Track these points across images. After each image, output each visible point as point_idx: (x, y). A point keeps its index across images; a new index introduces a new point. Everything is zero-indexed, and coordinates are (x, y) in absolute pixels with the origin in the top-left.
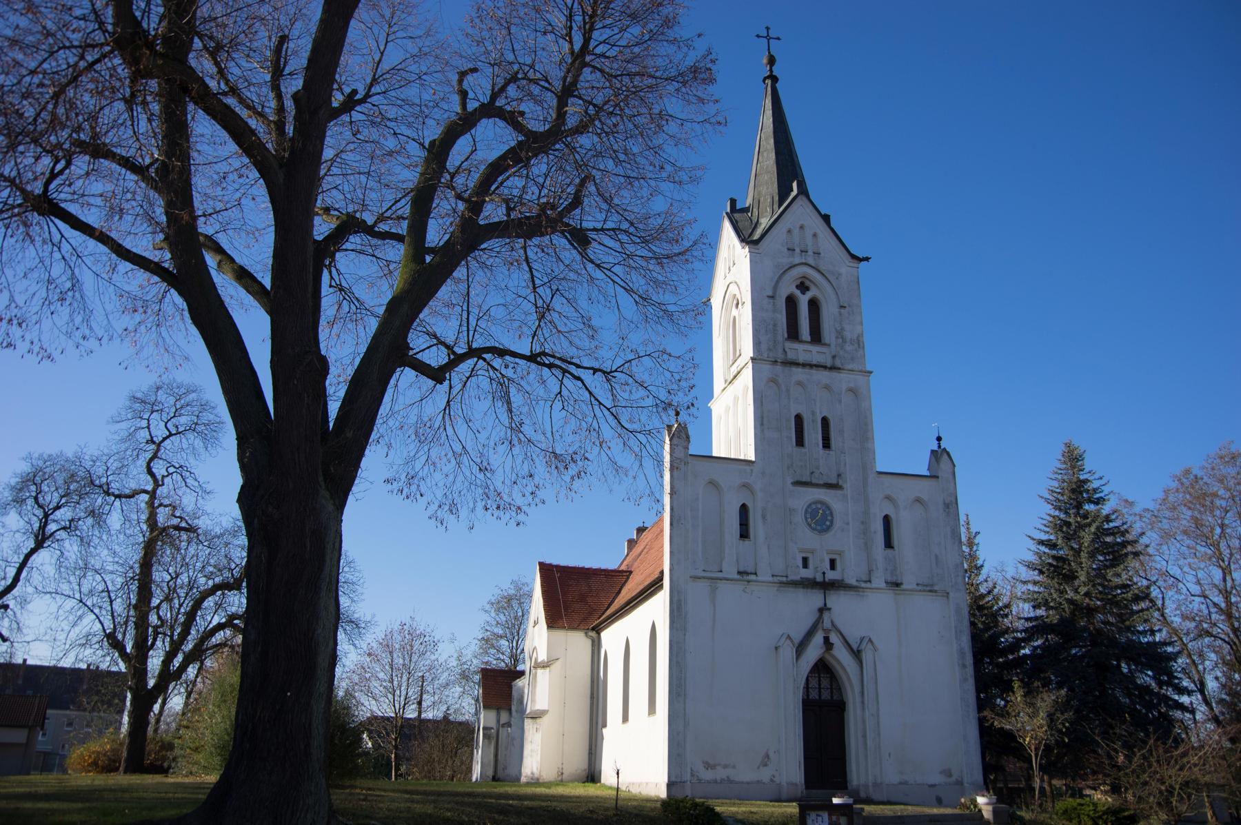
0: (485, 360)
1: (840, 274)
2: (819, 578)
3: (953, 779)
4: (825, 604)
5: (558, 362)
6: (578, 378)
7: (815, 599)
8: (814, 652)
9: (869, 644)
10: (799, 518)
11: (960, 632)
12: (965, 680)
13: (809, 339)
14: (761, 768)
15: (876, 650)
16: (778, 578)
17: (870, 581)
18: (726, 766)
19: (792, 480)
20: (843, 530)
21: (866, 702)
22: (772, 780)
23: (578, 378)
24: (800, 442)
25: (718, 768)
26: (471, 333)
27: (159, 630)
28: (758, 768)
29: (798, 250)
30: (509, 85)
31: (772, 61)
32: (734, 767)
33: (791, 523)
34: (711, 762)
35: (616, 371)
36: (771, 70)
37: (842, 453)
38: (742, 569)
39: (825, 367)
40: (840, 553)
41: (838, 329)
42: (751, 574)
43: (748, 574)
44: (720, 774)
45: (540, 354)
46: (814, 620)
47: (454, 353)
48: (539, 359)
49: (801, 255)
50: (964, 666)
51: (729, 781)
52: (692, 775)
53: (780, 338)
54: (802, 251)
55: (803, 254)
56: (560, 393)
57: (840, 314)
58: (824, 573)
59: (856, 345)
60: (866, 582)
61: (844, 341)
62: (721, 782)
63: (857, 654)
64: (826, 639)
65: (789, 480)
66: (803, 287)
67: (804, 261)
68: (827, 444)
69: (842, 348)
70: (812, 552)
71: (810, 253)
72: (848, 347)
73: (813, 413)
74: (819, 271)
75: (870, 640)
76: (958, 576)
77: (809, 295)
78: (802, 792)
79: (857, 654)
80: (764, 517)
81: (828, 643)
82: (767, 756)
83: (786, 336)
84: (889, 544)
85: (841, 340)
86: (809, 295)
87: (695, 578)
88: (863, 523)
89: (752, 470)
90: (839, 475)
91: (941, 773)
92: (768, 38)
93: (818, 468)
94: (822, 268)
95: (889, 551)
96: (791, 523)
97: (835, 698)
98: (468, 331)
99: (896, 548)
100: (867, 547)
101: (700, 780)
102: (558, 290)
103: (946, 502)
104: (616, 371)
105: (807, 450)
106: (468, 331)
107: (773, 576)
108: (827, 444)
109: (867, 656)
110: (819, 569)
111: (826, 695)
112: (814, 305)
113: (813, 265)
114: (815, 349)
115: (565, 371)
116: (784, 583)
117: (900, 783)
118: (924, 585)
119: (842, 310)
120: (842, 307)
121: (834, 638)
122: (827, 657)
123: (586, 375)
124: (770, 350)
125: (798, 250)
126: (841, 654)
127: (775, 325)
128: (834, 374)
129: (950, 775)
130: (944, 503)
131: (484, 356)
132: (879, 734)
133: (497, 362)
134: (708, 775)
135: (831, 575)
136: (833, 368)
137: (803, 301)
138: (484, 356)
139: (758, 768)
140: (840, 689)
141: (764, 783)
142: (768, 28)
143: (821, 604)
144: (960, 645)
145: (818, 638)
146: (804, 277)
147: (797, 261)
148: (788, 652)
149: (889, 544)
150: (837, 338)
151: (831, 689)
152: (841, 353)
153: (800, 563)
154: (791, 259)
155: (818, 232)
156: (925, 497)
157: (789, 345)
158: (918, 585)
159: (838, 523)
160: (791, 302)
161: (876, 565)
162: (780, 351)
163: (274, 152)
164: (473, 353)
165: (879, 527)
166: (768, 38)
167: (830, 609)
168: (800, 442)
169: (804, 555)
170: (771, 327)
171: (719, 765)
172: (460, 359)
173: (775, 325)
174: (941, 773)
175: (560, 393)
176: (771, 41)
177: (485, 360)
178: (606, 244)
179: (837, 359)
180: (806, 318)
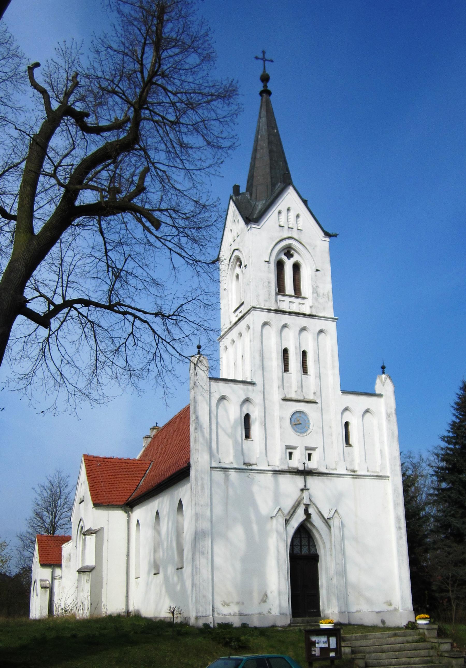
0: (76, 309)
1: (316, 246)
2: (301, 468)
4: (305, 486)
5: (129, 310)
6: (146, 322)
7: (299, 481)
8: (300, 517)
11: (397, 504)
12: (401, 538)
14: (262, 603)
23: (146, 322)
24: (286, 368)
26: (64, 288)
27: (199, 355)
30: (33, 75)
31: (265, 79)
35: (173, 315)
36: (265, 86)
39: (304, 315)
45: (115, 305)
47: (53, 304)
48: (115, 308)
49: (289, 230)
50: (400, 528)
54: (289, 228)
55: (290, 229)
56: (132, 333)
57: (316, 276)
58: (304, 464)
59: (327, 299)
61: (318, 295)
62: (234, 615)
63: (326, 521)
64: (306, 511)
66: (289, 255)
67: (290, 235)
71: (295, 229)
72: (321, 300)
74: (300, 243)
77: (293, 260)
78: (291, 620)
86: (293, 260)
92: (264, 60)
98: (63, 287)
102: (130, 256)
103: (389, 413)
104: (173, 315)
106: (63, 287)
109: (335, 523)
111: (305, 551)
112: (296, 267)
113: (297, 238)
114: (297, 301)
115: (135, 317)
118: (372, 472)
119: (317, 273)
120: (317, 270)
121: (311, 511)
122: (306, 523)
123: (149, 318)
124: (265, 301)
125: (286, 227)
126: (315, 519)
128: (311, 320)
129: (390, 605)
130: (387, 414)
131: (75, 305)
133: (84, 310)
138: (75, 305)
141: (264, 615)
142: (264, 52)
143: (302, 486)
150: (313, 293)
160: (280, 265)
164: (68, 304)
166: (264, 60)
167: (308, 489)
170: (267, 283)
172: (58, 308)
175: (132, 333)
176: (266, 62)
177: (76, 309)
179: (313, 308)
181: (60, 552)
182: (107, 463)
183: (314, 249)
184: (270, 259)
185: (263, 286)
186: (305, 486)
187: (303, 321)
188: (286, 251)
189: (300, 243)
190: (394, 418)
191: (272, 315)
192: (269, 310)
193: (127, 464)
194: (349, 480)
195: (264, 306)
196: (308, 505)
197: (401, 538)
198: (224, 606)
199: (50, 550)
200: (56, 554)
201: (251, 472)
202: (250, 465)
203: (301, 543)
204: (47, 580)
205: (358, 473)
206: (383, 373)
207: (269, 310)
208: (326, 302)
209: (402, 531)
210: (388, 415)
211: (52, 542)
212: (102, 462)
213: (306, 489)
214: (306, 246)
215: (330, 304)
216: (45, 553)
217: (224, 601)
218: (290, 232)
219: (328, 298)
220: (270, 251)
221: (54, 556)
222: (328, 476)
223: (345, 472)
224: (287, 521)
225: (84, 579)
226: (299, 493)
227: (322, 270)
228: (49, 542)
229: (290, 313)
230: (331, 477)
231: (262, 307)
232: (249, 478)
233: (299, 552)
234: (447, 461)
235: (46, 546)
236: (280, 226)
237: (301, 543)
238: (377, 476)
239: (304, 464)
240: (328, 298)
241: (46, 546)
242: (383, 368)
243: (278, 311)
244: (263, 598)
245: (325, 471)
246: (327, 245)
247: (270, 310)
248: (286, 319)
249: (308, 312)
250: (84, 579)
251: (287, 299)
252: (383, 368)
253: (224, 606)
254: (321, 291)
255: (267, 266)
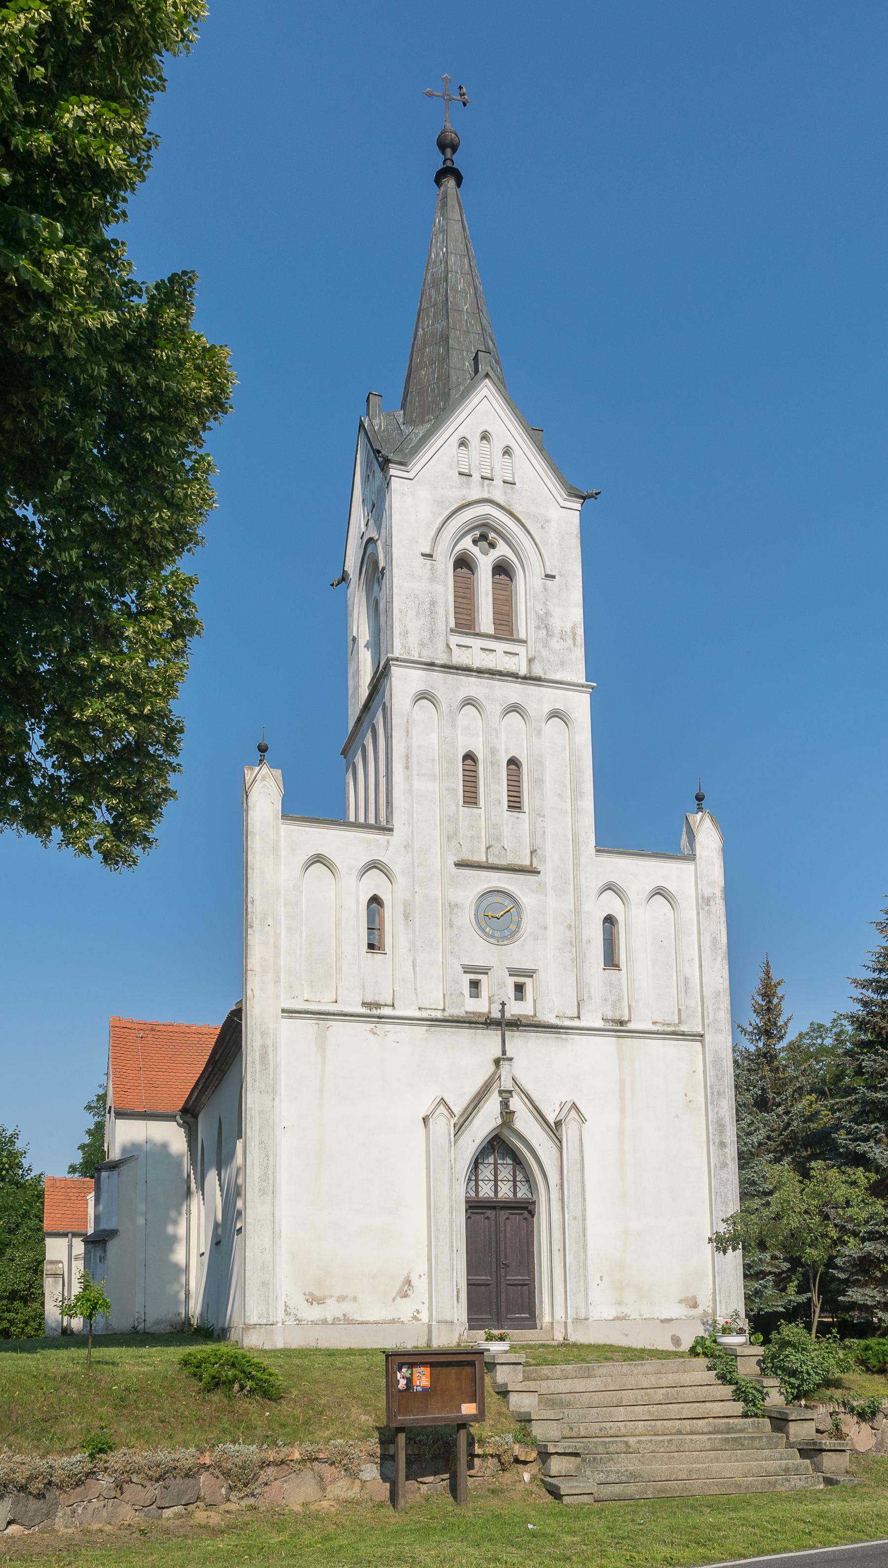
1: (547, 521)
3: (699, 1311)
4: (504, 1052)
9: (573, 1112)
10: (466, 917)
11: (719, 1093)
13: (491, 631)
14: (398, 1298)
15: (583, 1120)
16: (430, 1012)
17: (579, 1017)
18: (342, 1299)
19: (456, 859)
20: (536, 938)
21: (566, 1199)
22: (415, 1318)
24: (471, 798)
25: (329, 1301)
28: (394, 1299)
29: (476, 476)
32: (355, 1299)
33: (451, 926)
34: (317, 1293)
37: (539, 815)
38: (368, 1000)
39: (515, 676)
40: (529, 974)
41: (541, 613)
42: (386, 1005)
43: (451, 1165)
44: (332, 1310)
46: (487, 1076)
50: (722, 1145)
51: (347, 1321)
52: (287, 1313)
53: (441, 627)
54: (483, 478)
55: (487, 482)
57: (545, 589)
58: (503, 1004)
59: (570, 642)
60: (572, 1018)
61: (550, 633)
63: (555, 1129)
64: (505, 1104)
65: (451, 860)
67: (486, 496)
68: (515, 805)
69: (546, 645)
70: (485, 971)
71: (498, 482)
72: (556, 644)
73: (493, 751)
74: (511, 514)
75: (574, 1106)
76: (719, 1009)
77: (494, 555)
79: (555, 1129)
80: (406, 916)
81: (507, 1114)
82: (408, 1282)
83: (452, 623)
84: (611, 960)
85: (545, 632)
87: (289, 1013)
88: (570, 927)
89: (388, 842)
90: (533, 852)
91: (680, 1302)
93: (498, 840)
94: (517, 509)
95: (612, 973)
96: (451, 926)
97: (519, 1195)
99: (623, 965)
100: (578, 962)
101: (299, 1322)
105: (482, 811)
107: (420, 1009)
108: (515, 805)
109: (569, 1132)
110: (496, 998)
112: (502, 569)
113: (502, 503)
114: (501, 647)
116: (437, 1020)
117: (617, 1318)
118: (664, 1024)
119: (549, 582)
121: (516, 1103)
122: (506, 1133)
124: (422, 644)
125: (476, 476)
127: (433, 603)
128: (532, 690)
129: (695, 1305)
132: (585, 1246)
134: (313, 1313)
135: (515, 1009)
136: (530, 679)
137: (485, 563)
139: (394, 1299)
140: (504, 1142)
141: (402, 1322)
144: (717, 1113)
145: (493, 1104)
146: (484, 525)
147: (475, 495)
148: (442, 1126)
149: (611, 960)
150: (538, 628)
151: (515, 1181)
152: (544, 653)
153: (466, 989)
154: (465, 491)
155: (513, 445)
156: (671, 887)
157: (455, 639)
158: (654, 1023)
159: (528, 925)
161: (589, 992)
162: (441, 646)
163: (12, 148)
165: (595, 933)
168: (471, 798)
169: (473, 977)
170: (426, 606)
171: (331, 1297)
173: (433, 603)
174: (680, 1302)
178: (586, 1496)
180: (487, 595)
181: (85, 1206)
182: (159, 1033)
183: (542, 527)
184: (433, 549)
185: (418, 612)
186: (504, 1052)
187: (513, 692)
188: (477, 533)
189: (511, 514)
190: (719, 907)
191: (437, 676)
192: (431, 665)
193: (200, 1036)
194: (608, 1043)
195: (420, 657)
196: (510, 1092)
197: (724, 1165)
198: (312, 1304)
199: (68, 1205)
200: (80, 1213)
201: (378, 1023)
202: (378, 1006)
203: (496, 1175)
204: (61, 1262)
205: (631, 1026)
206: (700, 809)
207: (431, 665)
208: (569, 649)
209: (726, 1150)
210: (704, 902)
211: (74, 1190)
212: (147, 1032)
213: (504, 1059)
214: (524, 521)
215: (579, 653)
216: (57, 1211)
217: (311, 1294)
218: (486, 488)
219: (574, 640)
220: (433, 532)
221: (77, 1216)
222: (559, 1033)
223: (600, 1024)
224: (459, 1129)
225: (95, 1255)
226: (493, 1068)
227: (561, 576)
228: (69, 1190)
229: (480, 672)
230: (566, 1033)
231: (416, 658)
232: (374, 1034)
233: (492, 1195)
234: (160, 564)
235: (63, 1197)
236: (460, 474)
237: (496, 1175)
238: (674, 1033)
239: (503, 1004)
240: (574, 640)
241: (63, 1197)
242: (699, 798)
243: (449, 668)
244: (402, 1287)
245: (554, 1021)
246: (575, 518)
247: (432, 664)
248: (472, 686)
249: (523, 672)
250: (95, 1255)
251: (477, 643)
252: (699, 798)
253: (312, 1304)
254: (556, 623)
255: (429, 567)
